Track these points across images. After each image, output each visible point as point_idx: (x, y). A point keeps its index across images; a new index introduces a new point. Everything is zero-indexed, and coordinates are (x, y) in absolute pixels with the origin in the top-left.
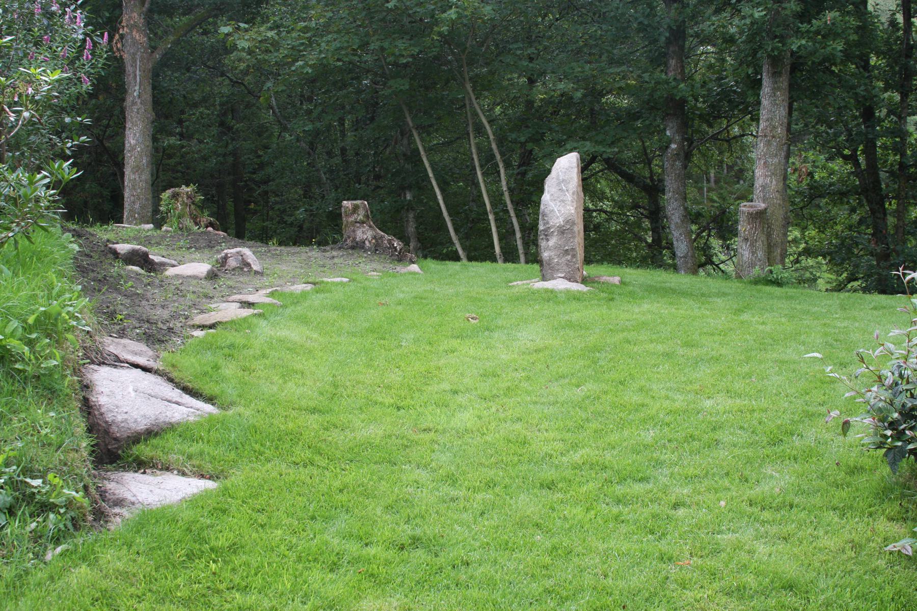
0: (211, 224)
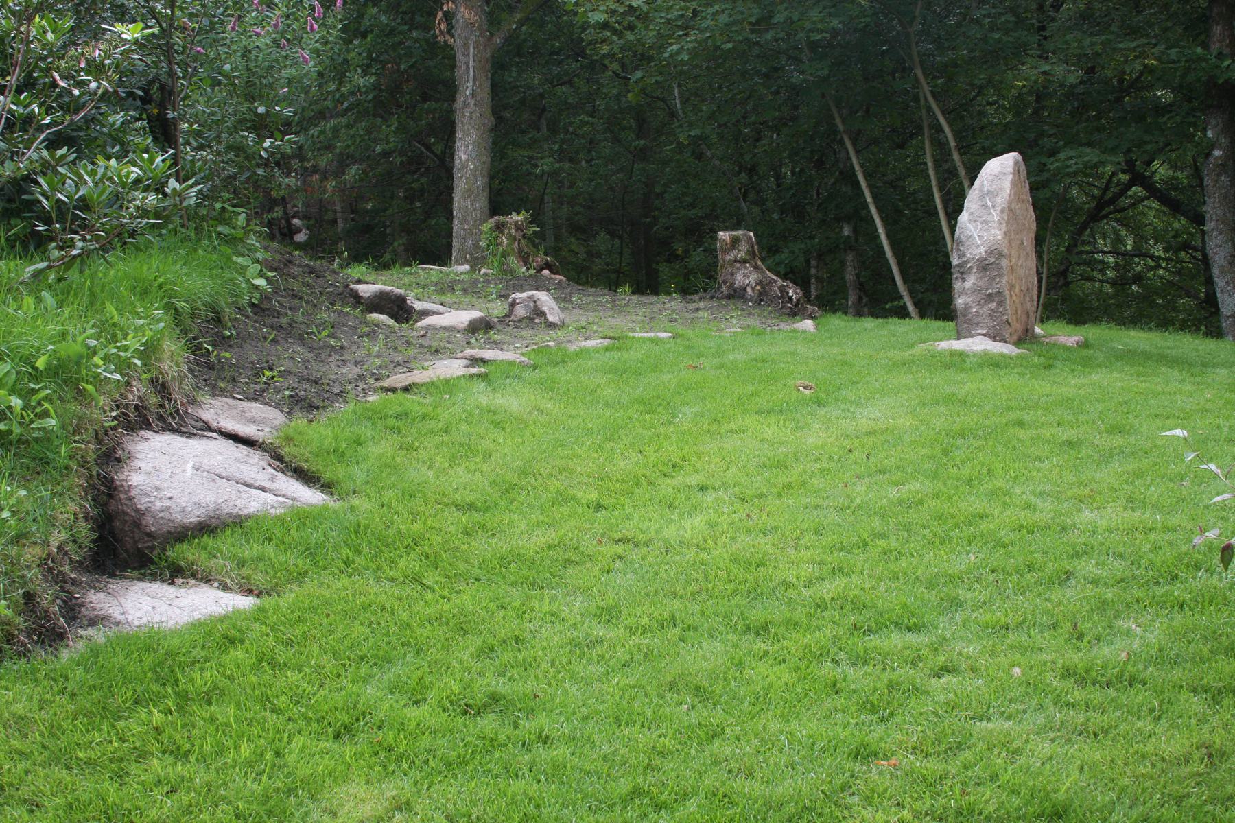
0: (547, 266)
